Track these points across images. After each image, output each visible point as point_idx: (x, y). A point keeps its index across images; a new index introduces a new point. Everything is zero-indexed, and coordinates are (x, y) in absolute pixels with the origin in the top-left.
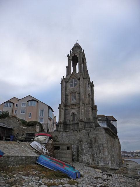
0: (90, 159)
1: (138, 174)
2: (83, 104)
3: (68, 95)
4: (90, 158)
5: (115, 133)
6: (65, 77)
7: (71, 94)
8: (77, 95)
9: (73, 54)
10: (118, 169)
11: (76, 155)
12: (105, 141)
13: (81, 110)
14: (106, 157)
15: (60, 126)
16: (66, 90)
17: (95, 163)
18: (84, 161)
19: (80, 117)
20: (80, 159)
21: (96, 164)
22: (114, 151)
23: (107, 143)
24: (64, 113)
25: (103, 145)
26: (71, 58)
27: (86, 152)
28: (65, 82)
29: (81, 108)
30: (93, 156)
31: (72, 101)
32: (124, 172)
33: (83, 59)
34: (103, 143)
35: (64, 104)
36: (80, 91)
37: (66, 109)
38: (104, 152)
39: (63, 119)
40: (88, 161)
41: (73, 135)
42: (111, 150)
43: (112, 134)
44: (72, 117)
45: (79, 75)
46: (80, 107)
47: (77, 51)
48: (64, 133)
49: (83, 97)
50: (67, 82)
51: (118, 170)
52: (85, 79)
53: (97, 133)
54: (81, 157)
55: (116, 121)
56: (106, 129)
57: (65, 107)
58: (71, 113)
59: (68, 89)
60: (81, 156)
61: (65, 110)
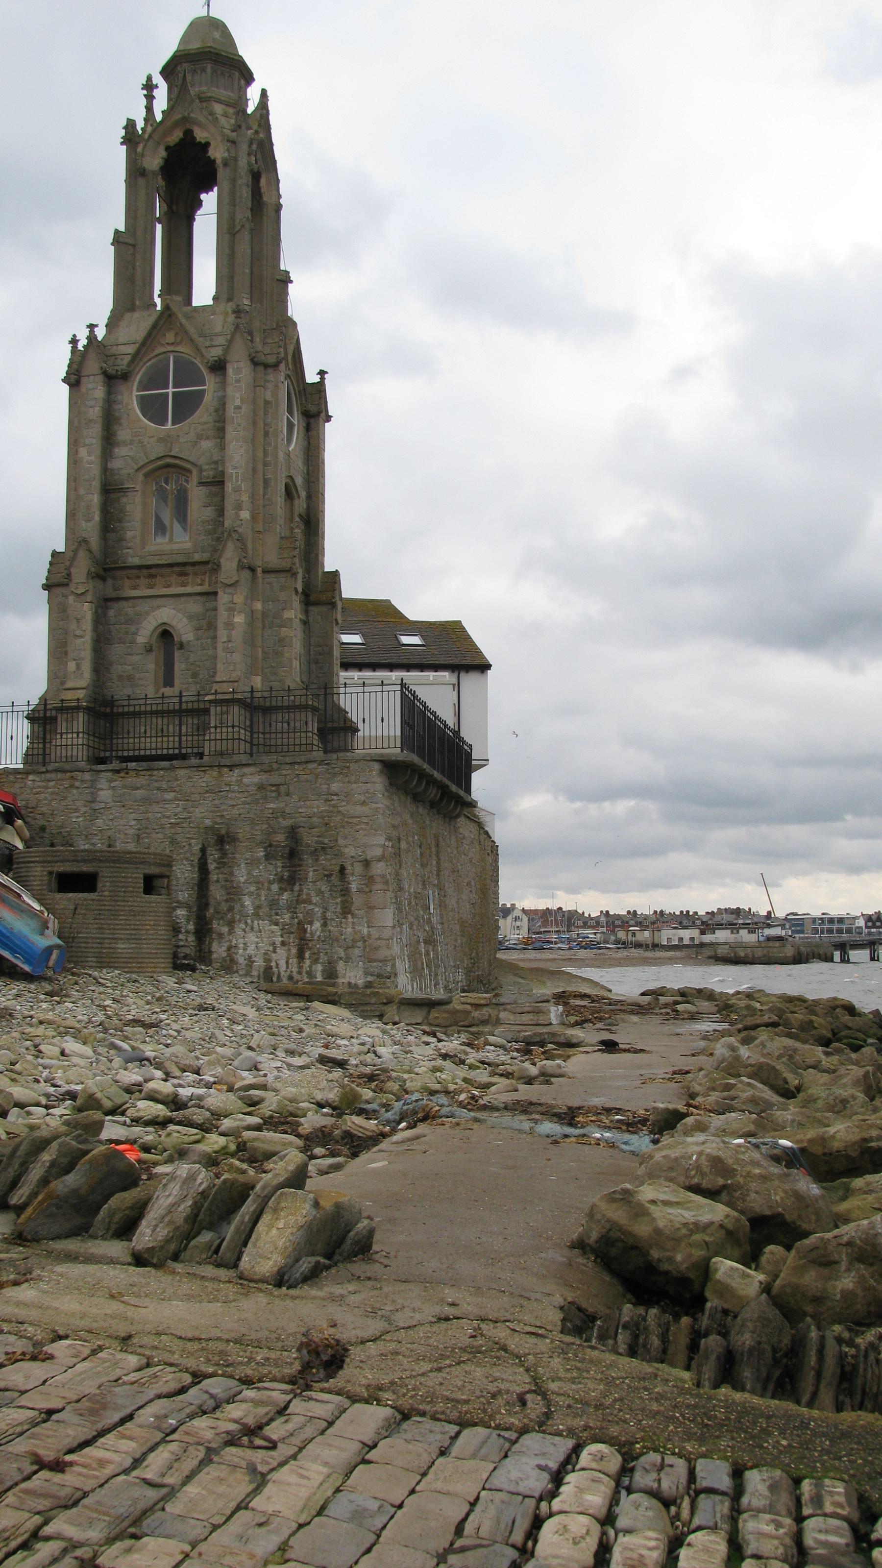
0: (282, 953)
1: (551, 1024)
2: (247, 574)
3: (123, 490)
4: (283, 944)
5: (454, 788)
6: (100, 333)
7: (146, 476)
8: (197, 495)
9: (176, 125)
10: (447, 1002)
11: (191, 927)
12: (381, 840)
13: (223, 614)
14: (385, 933)
15: (62, 726)
16: (109, 440)
17: (310, 974)
18: (241, 960)
19: (220, 667)
20: (219, 950)
21: (319, 978)
22: (442, 905)
23: (398, 854)
24: (95, 629)
25: (367, 863)
26: (154, 161)
27: (258, 907)
28: (105, 373)
29: (223, 598)
30: (305, 931)
31: (151, 538)
32: (476, 1014)
33: (256, 177)
34: (370, 855)
35: (90, 551)
36: (222, 462)
37: (108, 600)
38: (370, 908)
39: (86, 678)
40: (268, 960)
41: (170, 796)
42: (417, 896)
43: (433, 793)
44: (152, 657)
45: (221, 324)
46: (220, 594)
47: (208, 99)
48: (103, 783)
49: (245, 515)
50: (114, 379)
51: (448, 1007)
52: (266, 366)
53: (335, 787)
54: (221, 935)
55: (484, 667)
56: (392, 769)
57: (103, 579)
58: (146, 632)
59: (123, 434)
60: (225, 929)
61: (104, 603)
